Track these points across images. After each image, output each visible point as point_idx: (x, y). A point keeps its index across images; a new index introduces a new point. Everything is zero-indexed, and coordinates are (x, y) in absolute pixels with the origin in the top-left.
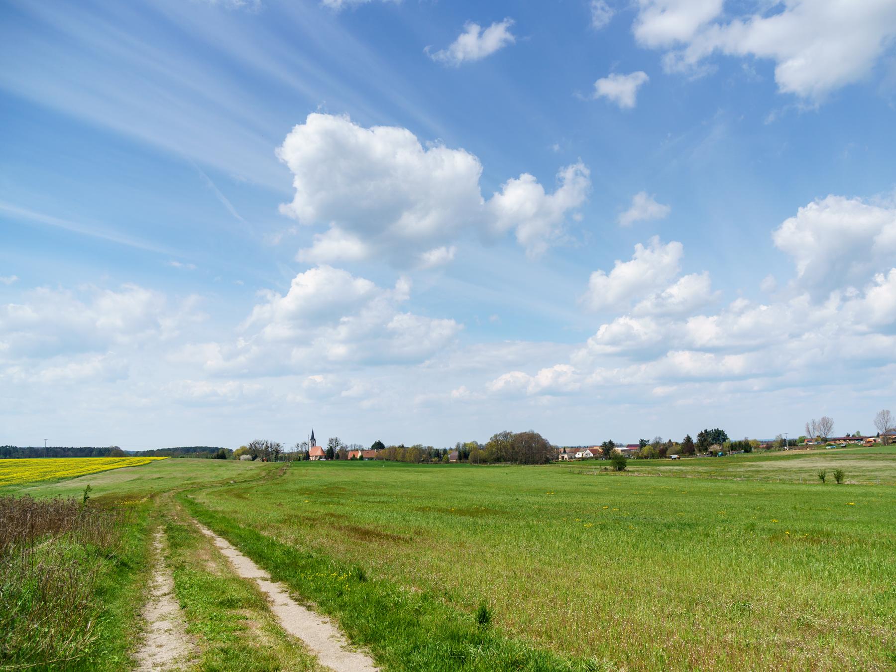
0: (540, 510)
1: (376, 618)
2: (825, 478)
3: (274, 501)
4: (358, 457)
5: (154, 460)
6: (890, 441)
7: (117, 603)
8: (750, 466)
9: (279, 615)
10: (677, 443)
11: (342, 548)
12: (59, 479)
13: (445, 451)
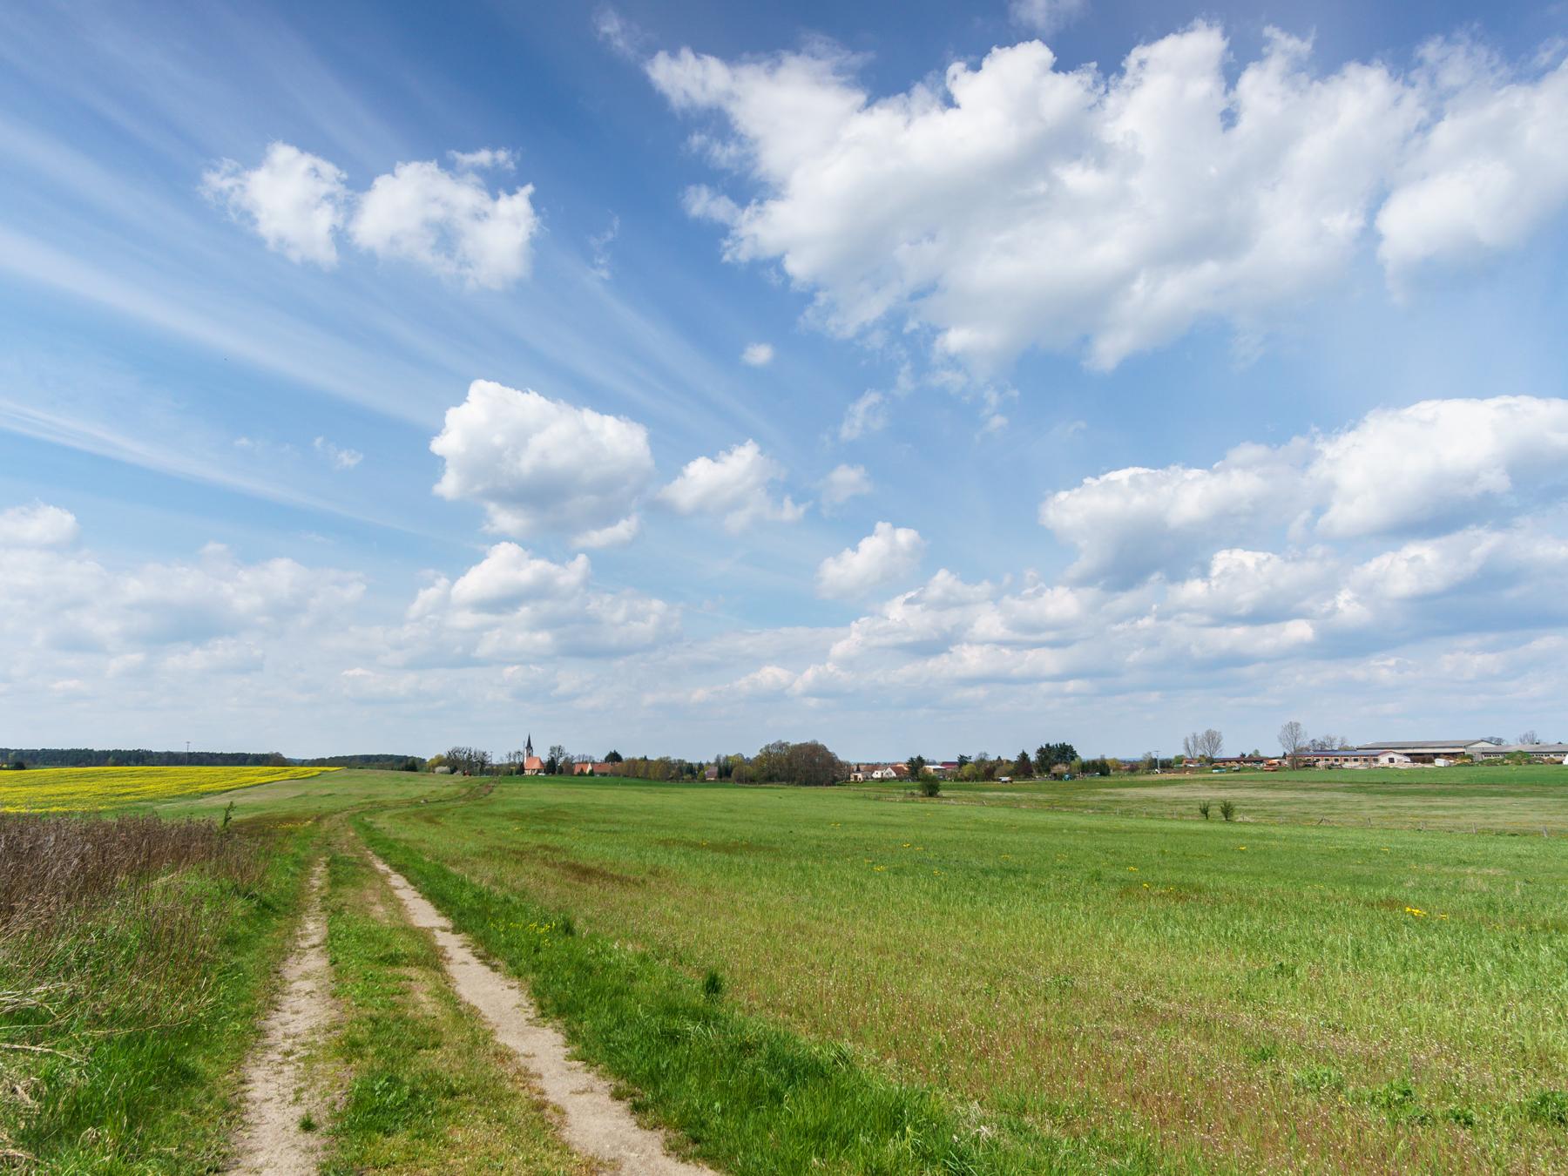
0: (819, 846)
1: (576, 983)
2: (1209, 813)
3: (475, 828)
4: (588, 771)
5: (324, 771)
6: (1302, 764)
7: (250, 955)
8: (1107, 794)
9: (455, 976)
10: (1008, 762)
11: (552, 891)
12: (202, 794)
13: (701, 766)
